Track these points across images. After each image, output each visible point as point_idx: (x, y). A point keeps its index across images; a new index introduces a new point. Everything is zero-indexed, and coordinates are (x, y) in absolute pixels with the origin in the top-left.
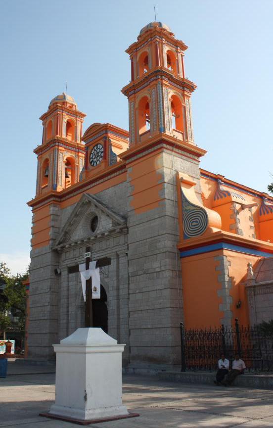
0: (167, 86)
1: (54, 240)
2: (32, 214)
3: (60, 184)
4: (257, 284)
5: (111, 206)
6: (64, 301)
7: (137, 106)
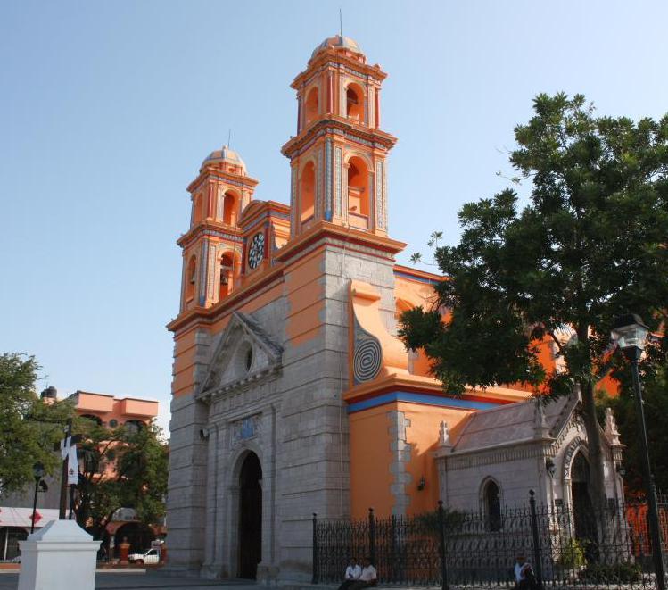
0: (342, 143)
1: (198, 383)
2: (174, 344)
3: (211, 295)
4: (454, 453)
5: (269, 333)
6: (211, 479)
7: (300, 176)
